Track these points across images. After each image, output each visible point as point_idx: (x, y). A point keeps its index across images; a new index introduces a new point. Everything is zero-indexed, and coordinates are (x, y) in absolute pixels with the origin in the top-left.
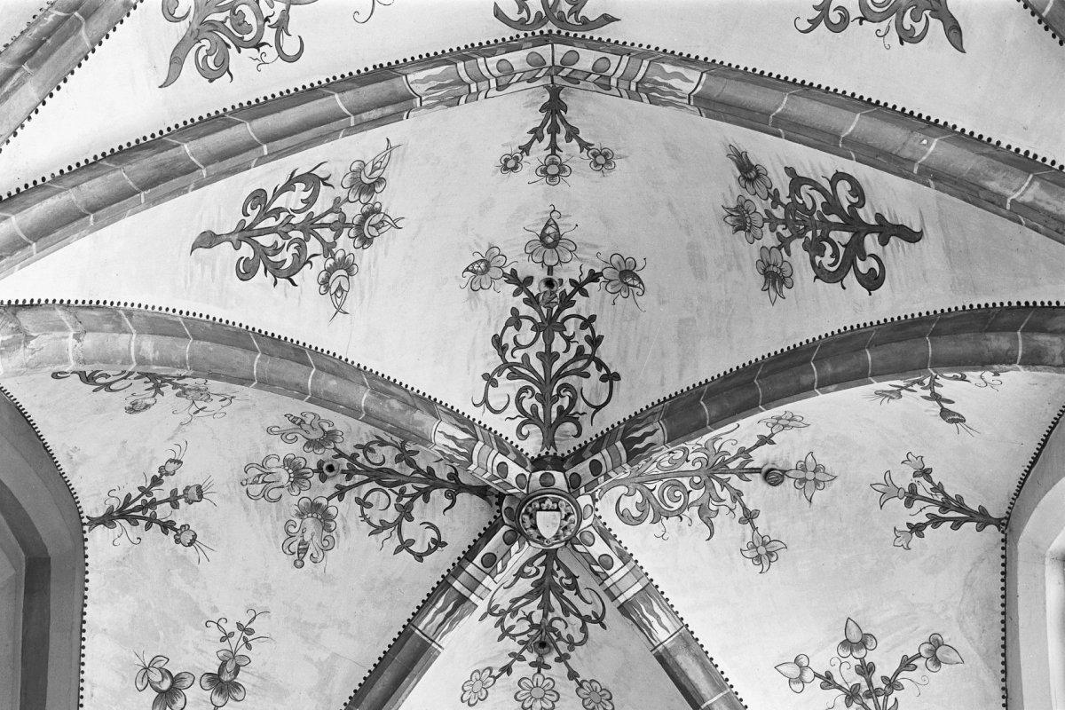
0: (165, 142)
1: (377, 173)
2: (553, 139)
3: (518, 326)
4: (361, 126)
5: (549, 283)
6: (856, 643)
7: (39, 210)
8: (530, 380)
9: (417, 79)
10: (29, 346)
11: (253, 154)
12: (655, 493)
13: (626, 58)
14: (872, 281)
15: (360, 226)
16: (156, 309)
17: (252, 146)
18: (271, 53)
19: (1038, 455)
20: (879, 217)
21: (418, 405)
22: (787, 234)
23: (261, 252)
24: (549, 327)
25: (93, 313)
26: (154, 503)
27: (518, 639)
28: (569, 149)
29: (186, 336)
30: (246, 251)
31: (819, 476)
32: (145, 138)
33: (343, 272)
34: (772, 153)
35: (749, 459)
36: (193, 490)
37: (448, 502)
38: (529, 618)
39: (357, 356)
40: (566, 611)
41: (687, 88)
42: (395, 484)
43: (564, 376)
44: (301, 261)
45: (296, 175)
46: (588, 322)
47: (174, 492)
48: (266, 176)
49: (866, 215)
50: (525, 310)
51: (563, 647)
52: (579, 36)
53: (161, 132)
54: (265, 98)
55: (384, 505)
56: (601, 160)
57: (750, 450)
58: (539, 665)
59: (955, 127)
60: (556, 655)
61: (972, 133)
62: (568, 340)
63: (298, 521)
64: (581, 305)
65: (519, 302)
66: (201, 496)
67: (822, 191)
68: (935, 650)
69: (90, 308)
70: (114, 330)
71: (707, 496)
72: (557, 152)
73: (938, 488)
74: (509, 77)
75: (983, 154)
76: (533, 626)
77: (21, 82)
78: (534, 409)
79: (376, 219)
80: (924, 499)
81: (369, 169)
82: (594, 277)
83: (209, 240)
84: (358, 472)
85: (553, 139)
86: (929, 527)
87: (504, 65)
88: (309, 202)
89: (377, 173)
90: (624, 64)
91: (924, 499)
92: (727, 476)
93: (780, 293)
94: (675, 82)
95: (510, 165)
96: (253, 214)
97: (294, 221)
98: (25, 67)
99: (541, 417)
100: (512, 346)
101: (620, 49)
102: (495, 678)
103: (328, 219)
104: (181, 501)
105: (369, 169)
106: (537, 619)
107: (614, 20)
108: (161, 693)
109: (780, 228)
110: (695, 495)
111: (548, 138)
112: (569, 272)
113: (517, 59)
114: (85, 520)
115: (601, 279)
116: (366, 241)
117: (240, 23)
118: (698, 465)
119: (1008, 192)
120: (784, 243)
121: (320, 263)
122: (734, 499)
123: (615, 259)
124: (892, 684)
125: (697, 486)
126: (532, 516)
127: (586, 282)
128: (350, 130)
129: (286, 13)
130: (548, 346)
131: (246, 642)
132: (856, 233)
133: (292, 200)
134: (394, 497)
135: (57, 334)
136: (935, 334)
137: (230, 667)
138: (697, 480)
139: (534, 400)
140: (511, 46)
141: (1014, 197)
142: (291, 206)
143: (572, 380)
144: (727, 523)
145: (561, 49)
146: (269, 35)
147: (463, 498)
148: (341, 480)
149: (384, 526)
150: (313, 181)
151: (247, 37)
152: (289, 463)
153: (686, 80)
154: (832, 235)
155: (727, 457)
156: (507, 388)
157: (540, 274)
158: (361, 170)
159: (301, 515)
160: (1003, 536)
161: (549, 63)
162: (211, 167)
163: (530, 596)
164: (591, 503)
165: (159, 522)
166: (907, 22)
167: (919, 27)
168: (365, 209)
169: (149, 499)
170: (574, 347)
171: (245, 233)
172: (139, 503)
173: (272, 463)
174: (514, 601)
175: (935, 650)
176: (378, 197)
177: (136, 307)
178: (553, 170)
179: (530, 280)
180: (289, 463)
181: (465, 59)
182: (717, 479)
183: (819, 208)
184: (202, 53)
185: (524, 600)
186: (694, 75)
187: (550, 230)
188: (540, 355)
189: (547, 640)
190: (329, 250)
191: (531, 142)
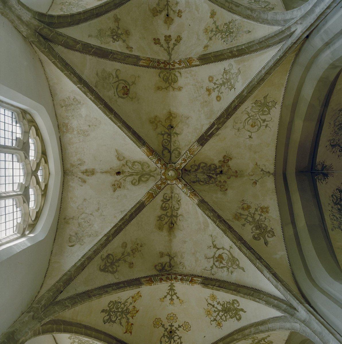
19: (51, 5)
27: (177, 334)
38: (174, 341)
51: (166, 334)
58: (171, 326)
60: (168, 330)
76: (173, 338)
102: (182, 326)
106: (172, 340)
189: (170, 334)
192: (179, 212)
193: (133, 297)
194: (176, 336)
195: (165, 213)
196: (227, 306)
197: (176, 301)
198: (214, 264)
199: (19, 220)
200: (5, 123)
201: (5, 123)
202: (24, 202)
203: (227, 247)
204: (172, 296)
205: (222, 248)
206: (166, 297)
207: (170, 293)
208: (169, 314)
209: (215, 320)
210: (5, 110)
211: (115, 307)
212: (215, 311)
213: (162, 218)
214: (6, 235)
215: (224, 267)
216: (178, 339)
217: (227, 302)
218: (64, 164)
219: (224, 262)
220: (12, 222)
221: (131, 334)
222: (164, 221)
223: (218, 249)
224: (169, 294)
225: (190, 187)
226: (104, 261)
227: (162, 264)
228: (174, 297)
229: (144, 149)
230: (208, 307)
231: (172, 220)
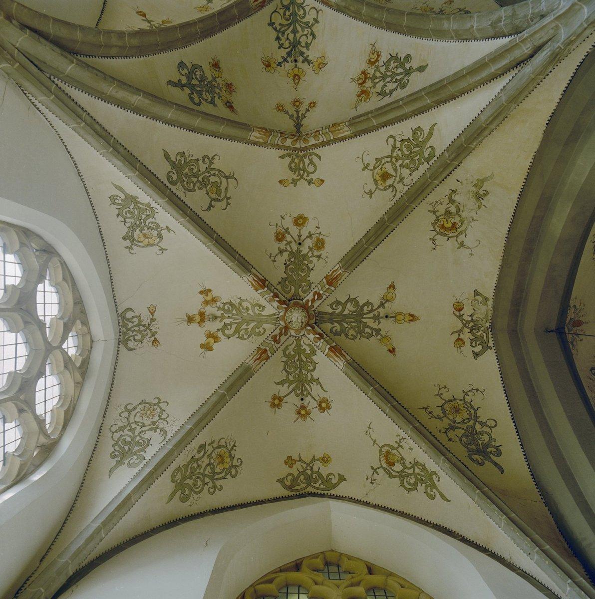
0: (436, 103)
1: (360, 98)
2: (298, 115)
3: (306, 43)
4: (367, 114)
5: (296, 61)
7: (484, 74)
8: (301, 22)
9: (347, 132)
10: (491, 21)
11: (405, 101)
13: (276, 144)
14: (181, 65)
15: (366, 78)
16: (442, 41)
17: (405, 104)
18: (398, 139)
20: (183, 90)
21: (343, 8)
22: (214, 83)
23: (402, 65)
24: (295, 45)
25: (466, 37)
28: (292, 111)
29: (431, 30)
30: (407, 66)
32: (443, 105)
33: (372, 60)
34: (224, 112)
39: (366, 27)
41: (254, 134)
43: (287, 25)
44: (387, 63)
45: (389, 96)
46: (281, 46)
48: (400, 94)
49: (187, 91)
50: (304, 50)
52: (291, 151)
53: (437, 107)
54: (400, 122)
56: (281, 108)
59: (163, 123)
61: (156, 121)
62: (288, 39)
64: (283, 53)
65: (307, 53)
67: (204, 99)
69: (467, 39)
70: (458, 31)
74: (315, 135)
75: (152, 113)
77: (486, 121)
78: (299, 10)
79: (360, 81)
81: (363, 99)
82: (280, 64)
83: (421, 69)
85: (298, 115)
87: (317, 139)
88: (384, 86)
89: (360, 98)
90: (276, 142)
93: (213, 60)
94: (259, 135)
95: (313, 104)
96: (405, 80)
97: (390, 78)
98: (484, 126)
101: (277, 147)
103: (378, 80)
105: (363, 99)
107: (280, 157)
109: (216, 85)
111: (300, 115)
112: (289, 65)
113: (313, 141)
115: (277, 63)
116: (363, 73)
117: (408, 148)
119: (142, 99)
120: (214, 79)
121: (380, 63)
123: (273, 71)
128: (371, 112)
129: (393, 152)
130: (295, 36)
132: (190, 84)
133: (390, 86)
135: (480, 27)
136: (157, 45)
139: (299, 13)
140: (315, 146)
141: (140, 97)
142: (391, 84)
143: (286, 23)
145: (297, 146)
146: (398, 144)
150: (382, 94)
151: (406, 143)
153: (255, 136)
154: (198, 83)
156: (309, 18)
157: (299, 64)
161: (301, 141)
162: (421, 95)
166: (183, 160)
167: (179, 158)
168: (364, 85)
170: (285, 36)
171: (408, 73)
177: (449, 41)
178: (297, 104)
179: (303, 62)
181: (331, 141)
183: (204, 93)
184: (422, 136)
186: (252, 138)
187: (297, 81)
188: (298, 32)
190: (377, 68)
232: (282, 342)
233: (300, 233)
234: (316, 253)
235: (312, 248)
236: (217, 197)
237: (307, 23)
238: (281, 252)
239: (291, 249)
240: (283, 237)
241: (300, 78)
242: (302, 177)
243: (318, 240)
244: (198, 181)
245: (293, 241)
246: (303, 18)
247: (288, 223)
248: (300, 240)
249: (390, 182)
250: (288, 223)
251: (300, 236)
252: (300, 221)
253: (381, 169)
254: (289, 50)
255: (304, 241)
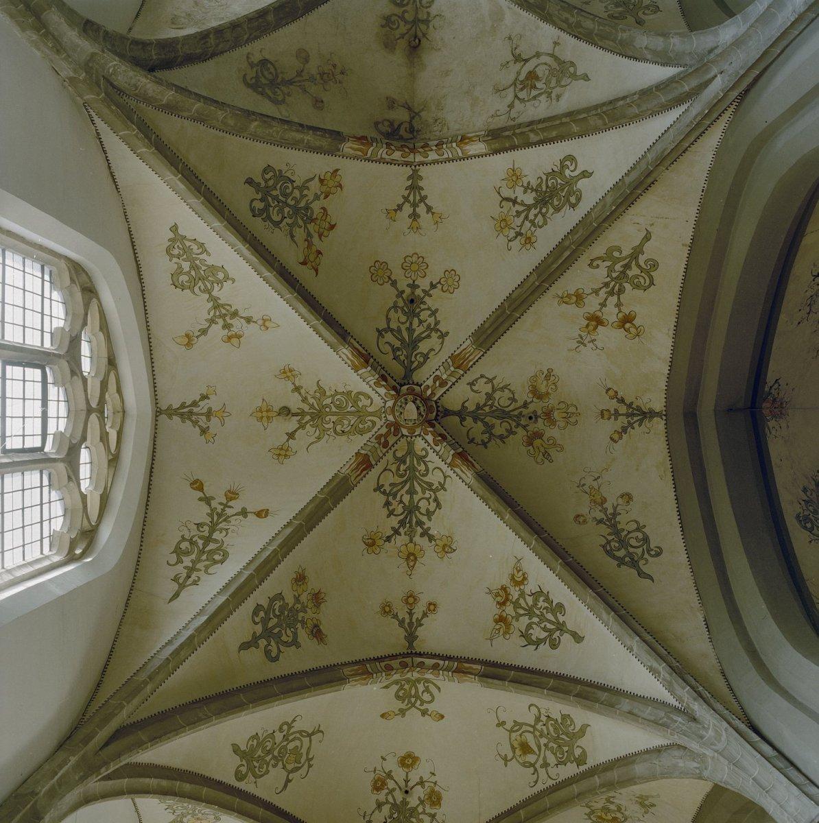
1: (498, 627)
2: (411, 620)
3: (428, 510)
6: (233, 338)
12: (351, 405)
24: (411, 509)
26: (628, 415)
27: (426, 307)
31: (260, 415)
35: (299, 421)
36: (606, 417)
37: (466, 404)
38: (421, 322)
40: (399, 330)
42: (494, 411)
46: (391, 513)
47: (616, 419)
50: (424, 519)
51: (401, 303)
55: (502, 399)
56: (387, 609)
57: (299, 428)
58: (413, 286)
60: (404, 296)
62: (401, 502)
63: (550, 391)
64: (394, 522)
66: (602, 411)
68: (189, 341)
71: (321, 400)
72: (409, 611)
73: (195, 423)
76: (418, 315)
78: (419, 464)
80: (202, 414)
84: (515, 416)
85: (411, 620)
86: (198, 400)
91: (202, 414)
92: (311, 411)
95: (432, 607)
99: (415, 459)
100: (431, 500)
102: (439, 282)
104: (613, 412)
106: (416, 321)
108: (630, 322)
110: (328, 401)
111: (414, 620)
112: (401, 540)
114: (664, 417)
115: (385, 539)
116: (504, 589)
118: (327, 419)
122: (306, 398)
124: (212, 321)
125: (327, 406)
126: (420, 414)
127: (392, 535)
130: (411, 498)
131: (581, 338)
134: (496, 404)
137: (591, 328)
138: (327, 410)
139: (419, 468)
143: (398, 480)
144: (309, 385)
146: (544, 719)
147: (457, 407)
148: (525, 411)
149: (502, 389)
152: (553, 422)
155: (311, 423)
157: (417, 539)
158: (505, 633)
159: (548, 393)
160: (158, 405)
163: (420, 339)
164: (387, 416)
165: (625, 404)
169: (630, 419)
172: (635, 419)
173: (562, 424)
174: (429, 336)
175: (189, 341)
176: (498, 612)
179: (422, 535)
180: (553, 422)
182: (316, 409)
185: (423, 335)
187: (412, 564)
189: (409, 305)
191: (422, 618)
192: (434, 10)
193: (321, 181)
194: (424, 310)
195: (398, 11)
196: (547, 187)
197: (425, 218)
198: (516, 96)
199: (58, 524)
200: (24, 327)
201: (24, 308)
202: (69, 478)
203: (546, 46)
204: (415, 205)
205: (534, 56)
206: (400, 207)
207: (411, 198)
208: (408, 256)
209: (519, 234)
210: (24, 258)
211: (278, 187)
212: (518, 213)
213: (393, 23)
214: (24, 559)
215: (540, 94)
216: (430, 316)
217: (547, 175)
218: (157, 427)
219: (539, 85)
220: (39, 510)
221: (317, 274)
222: (397, 31)
223: (526, 61)
224: (409, 202)
225: (454, 441)
226: (255, 69)
227: (391, 124)
228: (421, 209)
229: (346, 351)
230: (501, 210)
231: (416, 30)
232: (378, 390)
233: (407, 776)
234: (428, 810)
235: (424, 801)
236: (296, 765)
237: (430, 485)
238: (379, 805)
239: (394, 800)
240: (384, 784)
241: (416, 558)
242: (413, 705)
243: (433, 791)
244: (275, 757)
245: (398, 789)
246: (426, 475)
247: (392, 765)
248: (406, 786)
249: (531, 758)
250: (392, 765)
251: (407, 781)
252: (408, 761)
253: (521, 735)
254: (402, 517)
255: (413, 787)
